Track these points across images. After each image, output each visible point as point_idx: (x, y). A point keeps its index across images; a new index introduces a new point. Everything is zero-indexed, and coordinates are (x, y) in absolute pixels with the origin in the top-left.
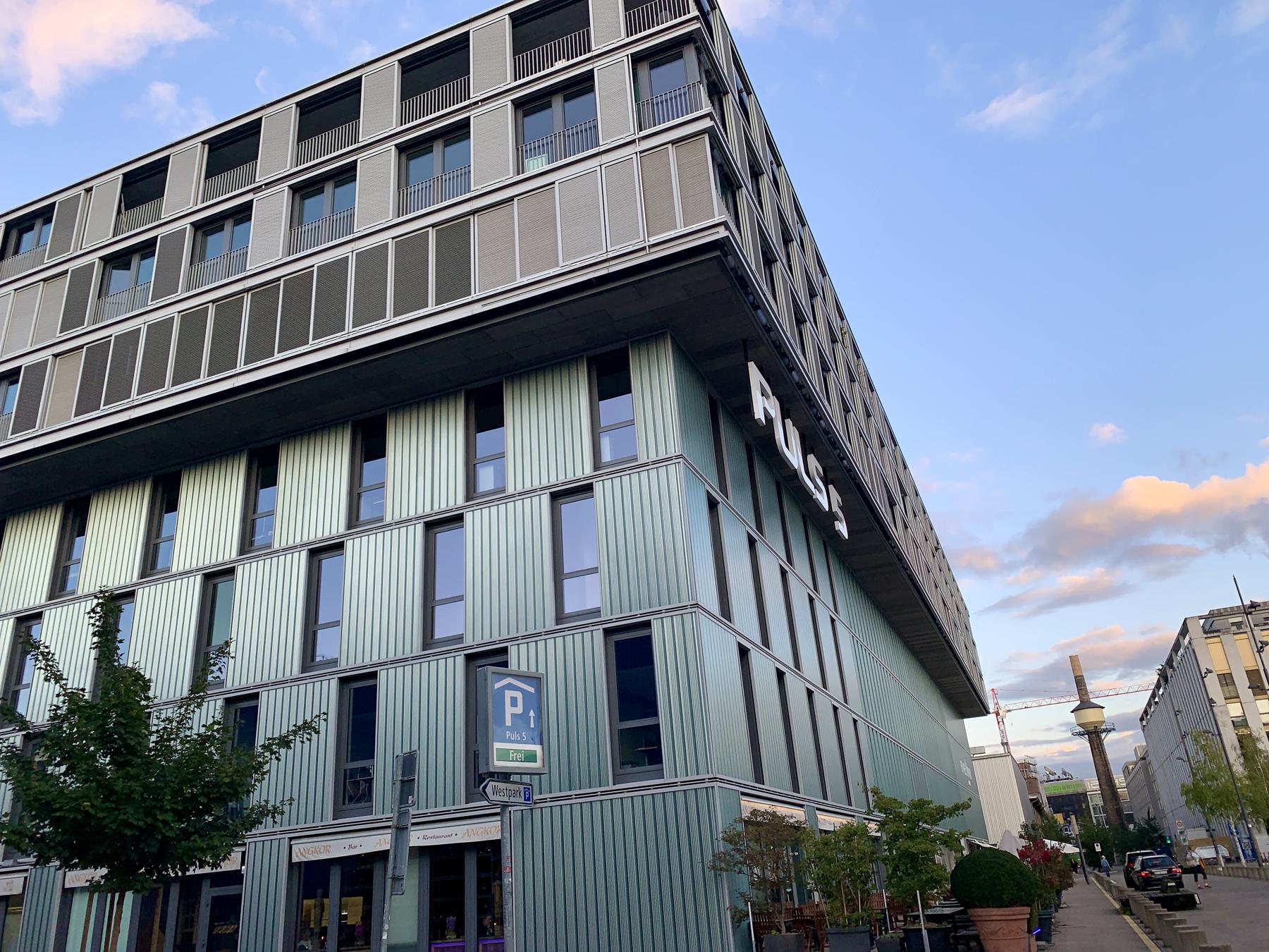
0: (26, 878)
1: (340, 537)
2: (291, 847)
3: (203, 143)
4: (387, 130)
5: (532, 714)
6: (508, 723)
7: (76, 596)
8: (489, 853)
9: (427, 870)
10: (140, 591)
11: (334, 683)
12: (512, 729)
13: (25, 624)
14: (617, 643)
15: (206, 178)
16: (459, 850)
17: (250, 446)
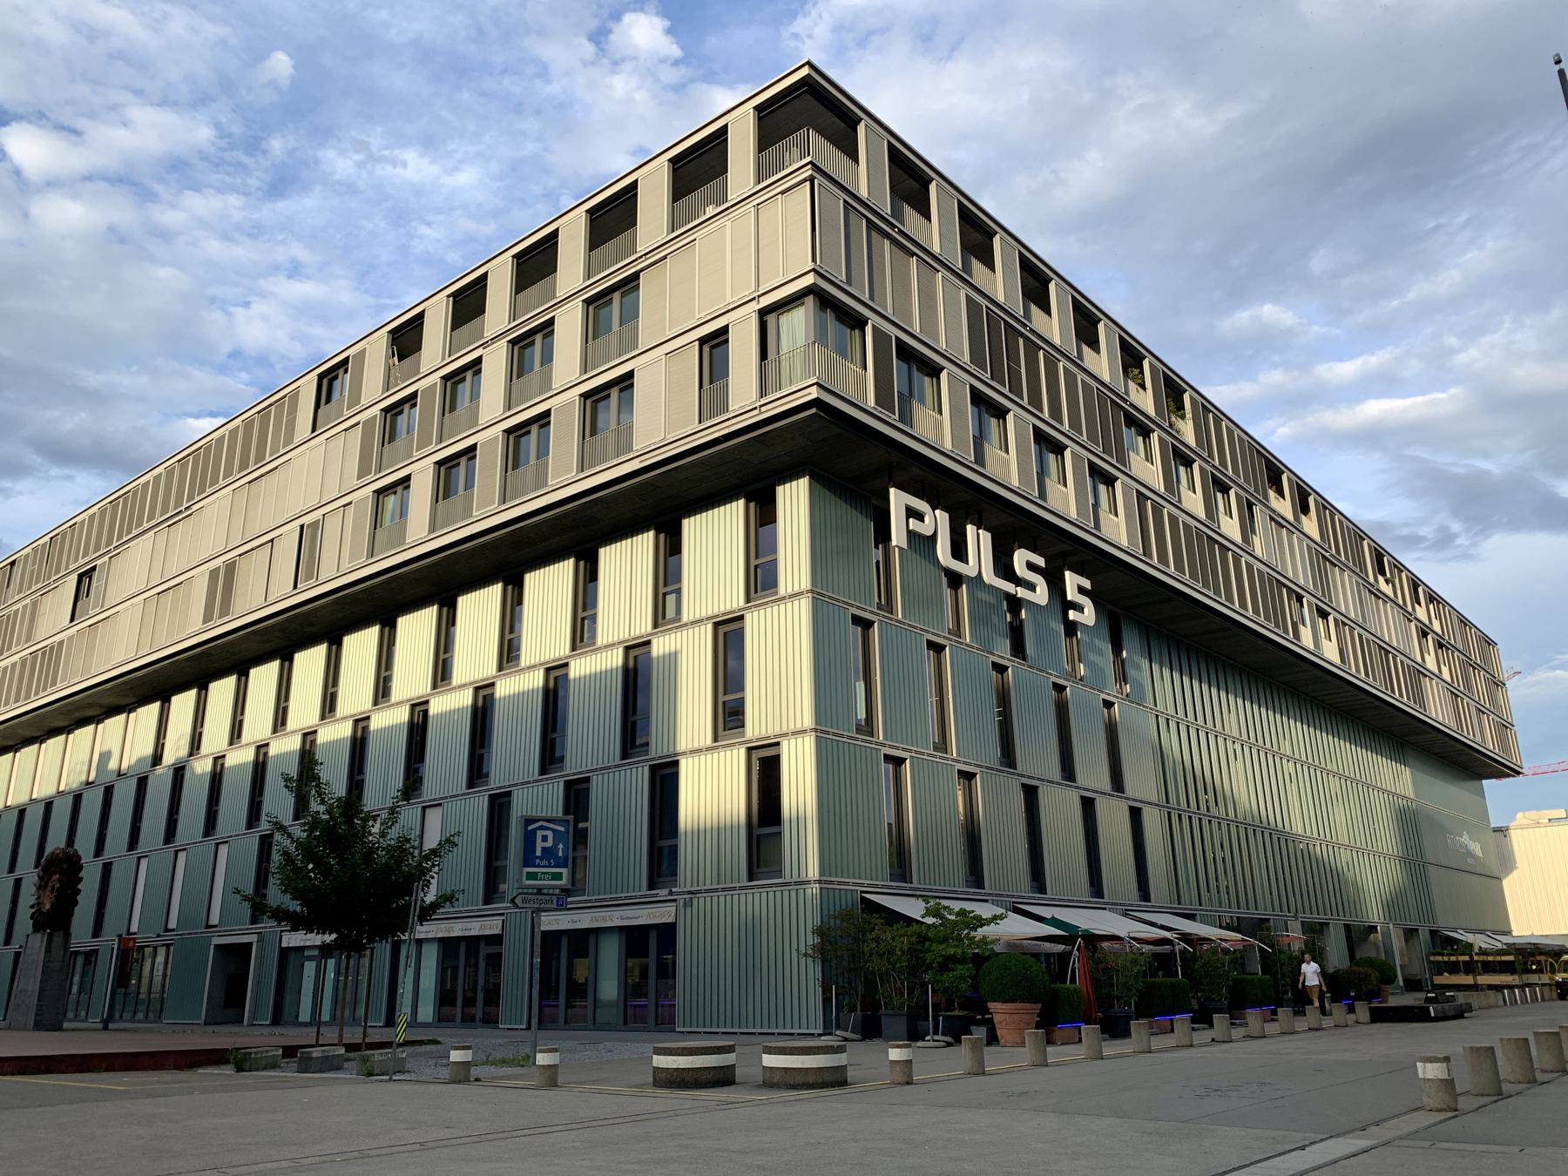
0: (503, 920)
2: (281, 937)
3: (448, 296)
5: (561, 846)
6: (538, 853)
7: (681, 623)
8: (667, 932)
9: (624, 940)
10: (370, 706)
12: (541, 858)
15: (452, 330)
16: (645, 929)
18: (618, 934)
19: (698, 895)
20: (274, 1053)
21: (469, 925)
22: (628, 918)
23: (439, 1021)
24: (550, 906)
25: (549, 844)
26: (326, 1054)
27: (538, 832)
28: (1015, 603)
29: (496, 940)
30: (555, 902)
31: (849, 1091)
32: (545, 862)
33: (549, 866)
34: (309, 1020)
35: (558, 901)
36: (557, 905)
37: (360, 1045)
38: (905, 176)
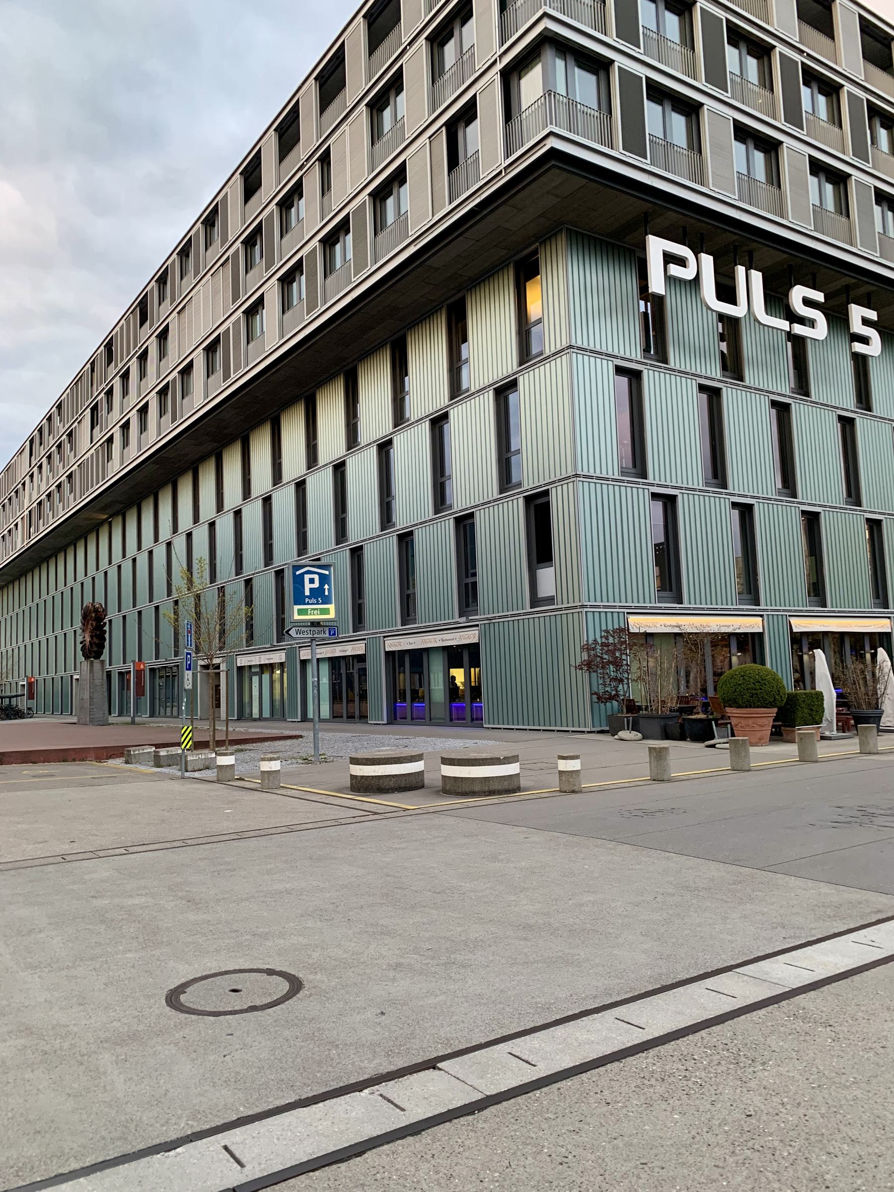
6: (307, 593)
12: (309, 597)
16: (403, 653)
18: (441, 654)
20: (149, 750)
23: (334, 717)
24: (322, 635)
25: (316, 585)
26: (170, 753)
28: (798, 343)
29: (361, 658)
30: (327, 632)
32: (313, 600)
33: (317, 604)
36: (330, 635)
37: (224, 741)
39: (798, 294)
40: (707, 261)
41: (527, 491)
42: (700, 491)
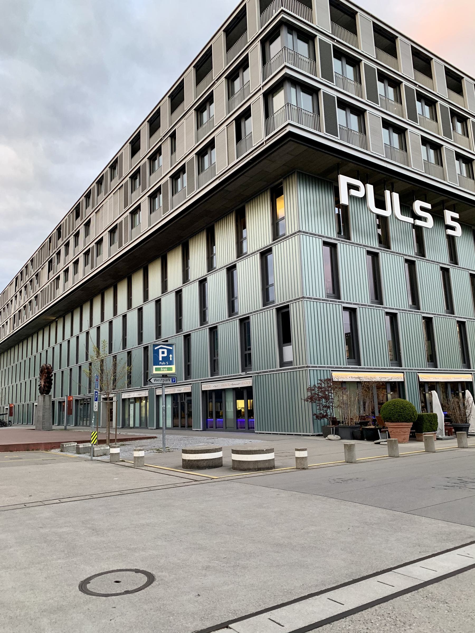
1: (270, 245)
4: (191, 103)
6: (160, 359)
7: (168, 292)
9: (235, 393)
11: (274, 311)
12: (162, 361)
13: (158, 303)
14: (282, 313)
17: (162, 255)
19: (260, 374)
21: (180, 389)
22: (234, 384)
23: (174, 427)
25: (165, 355)
27: (160, 350)
29: (189, 394)
30: (171, 380)
31: (272, 473)
32: (164, 363)
34: (133, 426)
35: (172, 380)
36: (172, 382)
37: (114, 440)
38: (342, 14)
39: (417, 205)
40: (370, 188)
41: (277, 305)
42: (369, 306)
